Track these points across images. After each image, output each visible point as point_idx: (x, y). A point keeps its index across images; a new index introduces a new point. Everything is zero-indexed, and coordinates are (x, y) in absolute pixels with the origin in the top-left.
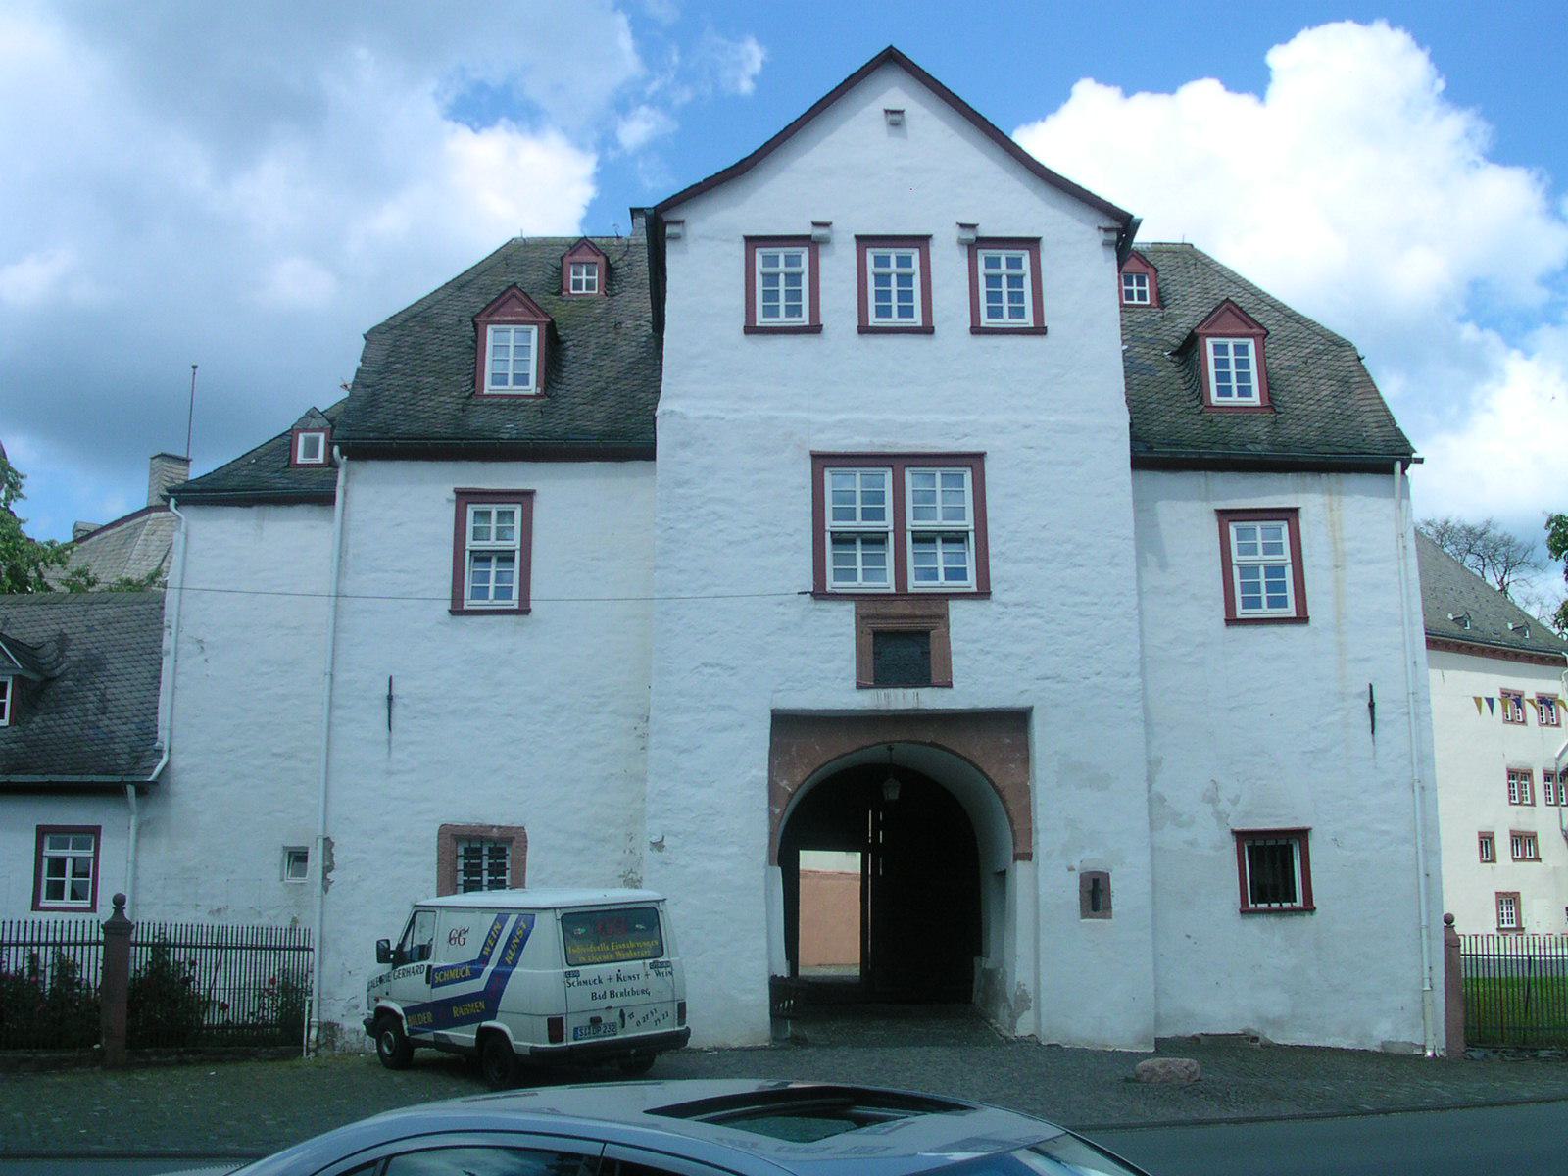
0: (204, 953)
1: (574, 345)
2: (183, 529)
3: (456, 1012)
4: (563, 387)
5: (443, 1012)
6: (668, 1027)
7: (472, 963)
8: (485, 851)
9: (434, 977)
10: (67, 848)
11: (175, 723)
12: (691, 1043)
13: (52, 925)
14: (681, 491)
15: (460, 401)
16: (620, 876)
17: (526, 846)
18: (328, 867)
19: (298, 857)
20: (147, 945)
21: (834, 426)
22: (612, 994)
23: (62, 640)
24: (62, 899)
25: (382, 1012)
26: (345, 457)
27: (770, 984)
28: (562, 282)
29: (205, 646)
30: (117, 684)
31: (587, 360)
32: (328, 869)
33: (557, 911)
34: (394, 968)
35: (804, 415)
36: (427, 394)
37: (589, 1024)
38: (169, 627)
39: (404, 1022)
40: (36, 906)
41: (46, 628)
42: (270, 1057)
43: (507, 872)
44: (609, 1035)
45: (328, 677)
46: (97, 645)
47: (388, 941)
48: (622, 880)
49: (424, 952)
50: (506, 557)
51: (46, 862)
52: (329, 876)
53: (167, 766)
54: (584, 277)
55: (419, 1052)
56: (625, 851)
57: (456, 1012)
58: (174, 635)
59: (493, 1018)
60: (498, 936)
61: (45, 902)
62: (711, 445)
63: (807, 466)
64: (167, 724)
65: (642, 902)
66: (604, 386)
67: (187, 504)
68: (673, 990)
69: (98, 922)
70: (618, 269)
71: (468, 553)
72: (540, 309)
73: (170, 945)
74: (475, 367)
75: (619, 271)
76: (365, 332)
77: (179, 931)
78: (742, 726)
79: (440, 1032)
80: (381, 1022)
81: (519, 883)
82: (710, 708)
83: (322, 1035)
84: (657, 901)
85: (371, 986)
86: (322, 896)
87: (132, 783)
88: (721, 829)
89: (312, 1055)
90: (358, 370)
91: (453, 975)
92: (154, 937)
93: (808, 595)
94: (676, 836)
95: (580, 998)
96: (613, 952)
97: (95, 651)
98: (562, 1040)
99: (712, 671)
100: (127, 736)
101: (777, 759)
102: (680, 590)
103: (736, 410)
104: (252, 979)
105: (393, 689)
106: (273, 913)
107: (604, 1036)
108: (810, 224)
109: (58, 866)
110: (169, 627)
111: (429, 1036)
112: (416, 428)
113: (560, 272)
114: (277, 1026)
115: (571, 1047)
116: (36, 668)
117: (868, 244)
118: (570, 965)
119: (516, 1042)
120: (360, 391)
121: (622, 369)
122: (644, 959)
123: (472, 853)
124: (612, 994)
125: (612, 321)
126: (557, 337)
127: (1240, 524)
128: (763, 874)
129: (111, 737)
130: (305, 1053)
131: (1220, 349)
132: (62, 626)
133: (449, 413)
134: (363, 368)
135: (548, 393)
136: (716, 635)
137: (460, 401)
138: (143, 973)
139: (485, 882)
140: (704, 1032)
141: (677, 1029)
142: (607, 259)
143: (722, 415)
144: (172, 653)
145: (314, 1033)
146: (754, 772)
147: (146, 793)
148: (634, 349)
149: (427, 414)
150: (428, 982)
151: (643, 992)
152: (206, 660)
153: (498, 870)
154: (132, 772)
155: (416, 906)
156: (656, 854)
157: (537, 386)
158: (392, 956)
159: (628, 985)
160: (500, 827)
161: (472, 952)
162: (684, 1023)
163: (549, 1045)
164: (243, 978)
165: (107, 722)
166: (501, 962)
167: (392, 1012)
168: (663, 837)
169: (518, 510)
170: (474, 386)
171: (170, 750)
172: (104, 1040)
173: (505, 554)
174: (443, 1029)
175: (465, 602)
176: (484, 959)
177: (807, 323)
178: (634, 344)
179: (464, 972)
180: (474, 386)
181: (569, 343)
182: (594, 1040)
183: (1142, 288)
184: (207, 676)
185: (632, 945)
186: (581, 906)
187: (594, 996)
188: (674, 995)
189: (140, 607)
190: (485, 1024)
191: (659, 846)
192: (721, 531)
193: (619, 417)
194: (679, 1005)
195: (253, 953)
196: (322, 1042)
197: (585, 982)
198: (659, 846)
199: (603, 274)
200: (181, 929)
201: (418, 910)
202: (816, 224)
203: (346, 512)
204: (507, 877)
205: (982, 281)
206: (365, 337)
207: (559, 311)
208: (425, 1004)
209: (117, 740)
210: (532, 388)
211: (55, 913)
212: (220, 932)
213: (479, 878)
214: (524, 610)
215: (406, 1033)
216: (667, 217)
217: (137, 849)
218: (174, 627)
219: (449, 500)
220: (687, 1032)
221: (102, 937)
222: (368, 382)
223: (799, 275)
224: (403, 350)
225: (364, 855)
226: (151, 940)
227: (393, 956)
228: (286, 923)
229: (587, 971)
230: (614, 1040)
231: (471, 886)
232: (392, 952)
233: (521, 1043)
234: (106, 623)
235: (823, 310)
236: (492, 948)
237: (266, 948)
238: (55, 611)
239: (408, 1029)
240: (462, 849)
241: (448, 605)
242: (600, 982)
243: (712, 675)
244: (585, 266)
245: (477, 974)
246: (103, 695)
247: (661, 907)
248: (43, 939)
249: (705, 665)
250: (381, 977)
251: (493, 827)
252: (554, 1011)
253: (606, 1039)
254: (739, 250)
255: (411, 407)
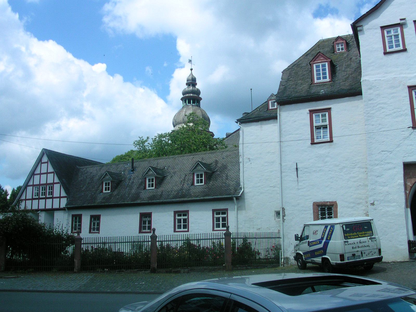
0: (258, 240)
1: (339, 66)
2: (242, 130)
3: (316, 253)
4: (336, 78)
5: (313, 254)
6: (376, 256)
7: (319, 240)
8: (326, 209)
9: (310, 244)
10: (220, 215)
11: (244, 181)
12: (383, 260)
13: (216, 234)
14: (370, 102)
15: (309, 86)
16: (364, 214)
17: (337, 207)
18: (284, 216)
19: (278, 213)
20: (242, 238)
21: (414, 77)
22: (358, 247)
23: (216, 162)
24: (181, 229)
25: (298, 254)
26: (279, 105)
27: (408, 242)
28: (334, 49)
29: (250, 160)
30: (230, 172)
31: (343, 70)
32: (284, 216)
33: (341, 224)
34: (300, 242)
35: (405, 75)
36: (299, 85)
37: (352, 256)
38: (241, 156)
39: (303, 257)
40: (175, 231)
41: (212, 159)
42: (271, 267)
43: (333, 214)
44: (358, 259)
45: (280, 164)
46: (225, 162)
47: (298, 235)
48: (365, 215)
49: (307, 237)
50: (325, 127)
51: (177, 220)
52: (284, 218)
53: (243, 191)
54: (340, 47)
55: (308, 265)
56: (365, 206)
57: (316, 253)
58: (242, 157)
59: (325, 255)
60: (326, 232)
61: (215, 229)
62: (378, 88)
63: (407, 90)
64: (242, 181)
65: (359, 221)
66: (348, 76)
67: (243, 123)
68: (377, 245)
69: (222, 233)
70: (350, 43)
71: (314, 127)
72: (328, 58)
73: (248, 238)
74: (312, 76)
75: (350, 44)
76: (282, 71)
77: (259, 234)
78: (394, 168)
79: (312, 259)
80: (298, 257)
81: (336, 217)
82: (385, 163)
83: (285, 261)
84: (371, 220)
85: (295, 247)
86: (283, 223)
87: (235, 197)
88: (390, 198)
89: (282, 266)
90: (281, 82)
91: (314, 243)
92: (243, 236)
93: (411, 128)
94: (377, 201)
95: (349, 249)
96: (358, 235)
97: (224, 164)
98: (344, 260)
99: (384, 153)
100: (233, 185)
101: (406, 177)
102: (373, 130)
103: (384, 77)
104: (269, 246)
105: (297, 166)
106: (273, 229)
107: (356, 259)
108: (399, 20)
109: (218, 219)
110: (241, 156)
111: (309, 260)
112: (297, 95)
113: (333, 47)
114: (274, 259)
115: (347, 262)
116: (210, 169)
117: (384, 28)
118: (345, 239)
119: (332, 261)
120: (282, 87)
121: (353, 71)
122: (367, 237)
123: (323, 210)
124: (358, 247)
125: (349, 58)
126: (334, 65)
127: (316, 114)
128: (404, 211)
129: (229, 185)
130: (280, 266)
131: (318, 67)
132: (216, 158)
133: (305, 90)
134: (282, 81)
135: (333, 80)
136: (385, 142)
137: (309, 86)
138: (241, 246)
139: (327, 217)
140: (387, 257)
141: (379, 256)
142: (346, 41)
143: (380, 79)
144: (242, 162)
145: (283, 260)
146: (399, 181)
147: (239, 199)
148: (356, 65)
149: (300, 91)
150: (308, 245)
151: (367, 246)
152: (251, 163)
153: (330, 214)
154: (234, 194)
155: (304, 225)
156: (372, 206)
157: (329, 79)
158: (299, 239)
159: (363, 244)
160: (329, 202)
161: (319, 237)
162: (381, 255)
163: (340, 262)
164: (266, 246)
165: (228, 182)
166: (327, 239)
167: (300, 254)
168: (374, 202)
169: (327, 114)
170: (312, 81)
171: (244, 188)
172: (226, 263)
173: (325, 126)
174: (313, 258)
175: (315, 140)
176: (322, 238)
177: (402, 49)
178: (356, 63)
179: (317, 242)
180: (312, 81)
181: (337, 66)
182: (354, 260)
183: (342, 47)
184: (252, 167)
185: (364, 233)
186: (349, 222)
187: (353, 248)
188: (377, 247)
189: (235, 152)
190: (323, 256)
191: (373, 204)
192: (383, 112)
193: (353, 84)
194: (379, 249)
195: (269, 240)
196: (285, 263)
197: (350, 244)
198: (373, 204)
199: (345, 46)
200: (260, 234)
201: (305, 226)
202: (401, 20)
203: (280, 120)
204: (333, 216)
205: (386, 39)
206: (282, 72)
207: (334, 58)
208: (308, 252)
209: (230, 186)
210: (328, 79)
211: (182, 233)
212: (255, 234)
213: (325, 216)
214: (331, 141)
215: (304, 259)
216: (357, 25)
217: (237, 214)
218: (242, 155)
219: (308, 113)
220: (382, 257)
221: (224, 237)
222: (283, 84)
223: (398, 35)
224: (292, 74)
225: (293, 212)
226: (242, 237)
227: (300, 239)
228: (277, 231)
229: (350, 241)
230: (360, 260)
231: (322, 218)
232: (299, 237)
233: (333, 262)
234: (227, 156)
235: (406, 44)
236: (324, 235)
237: (272, 238)
238: (215, 155)
239: (304, 258)
240: (327, 208)
241: (310, 142)
242: (354, 244)
243: (385, 154)
244: (340, 44)
245: (320, 243)
246: (227, 175)
247: (372, 222)
248: (214, 238)
249: (382, 151)
250: (297, 245)
251: (328, 202)
252: (341, 252)
253: (357, 260)
254: (379, 31)
255: (295, 89)
